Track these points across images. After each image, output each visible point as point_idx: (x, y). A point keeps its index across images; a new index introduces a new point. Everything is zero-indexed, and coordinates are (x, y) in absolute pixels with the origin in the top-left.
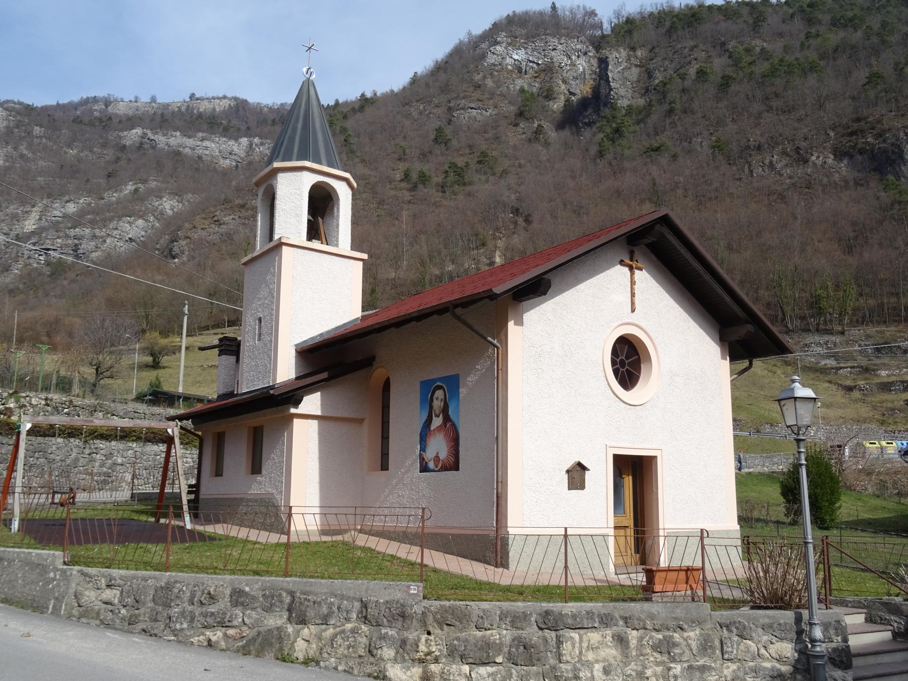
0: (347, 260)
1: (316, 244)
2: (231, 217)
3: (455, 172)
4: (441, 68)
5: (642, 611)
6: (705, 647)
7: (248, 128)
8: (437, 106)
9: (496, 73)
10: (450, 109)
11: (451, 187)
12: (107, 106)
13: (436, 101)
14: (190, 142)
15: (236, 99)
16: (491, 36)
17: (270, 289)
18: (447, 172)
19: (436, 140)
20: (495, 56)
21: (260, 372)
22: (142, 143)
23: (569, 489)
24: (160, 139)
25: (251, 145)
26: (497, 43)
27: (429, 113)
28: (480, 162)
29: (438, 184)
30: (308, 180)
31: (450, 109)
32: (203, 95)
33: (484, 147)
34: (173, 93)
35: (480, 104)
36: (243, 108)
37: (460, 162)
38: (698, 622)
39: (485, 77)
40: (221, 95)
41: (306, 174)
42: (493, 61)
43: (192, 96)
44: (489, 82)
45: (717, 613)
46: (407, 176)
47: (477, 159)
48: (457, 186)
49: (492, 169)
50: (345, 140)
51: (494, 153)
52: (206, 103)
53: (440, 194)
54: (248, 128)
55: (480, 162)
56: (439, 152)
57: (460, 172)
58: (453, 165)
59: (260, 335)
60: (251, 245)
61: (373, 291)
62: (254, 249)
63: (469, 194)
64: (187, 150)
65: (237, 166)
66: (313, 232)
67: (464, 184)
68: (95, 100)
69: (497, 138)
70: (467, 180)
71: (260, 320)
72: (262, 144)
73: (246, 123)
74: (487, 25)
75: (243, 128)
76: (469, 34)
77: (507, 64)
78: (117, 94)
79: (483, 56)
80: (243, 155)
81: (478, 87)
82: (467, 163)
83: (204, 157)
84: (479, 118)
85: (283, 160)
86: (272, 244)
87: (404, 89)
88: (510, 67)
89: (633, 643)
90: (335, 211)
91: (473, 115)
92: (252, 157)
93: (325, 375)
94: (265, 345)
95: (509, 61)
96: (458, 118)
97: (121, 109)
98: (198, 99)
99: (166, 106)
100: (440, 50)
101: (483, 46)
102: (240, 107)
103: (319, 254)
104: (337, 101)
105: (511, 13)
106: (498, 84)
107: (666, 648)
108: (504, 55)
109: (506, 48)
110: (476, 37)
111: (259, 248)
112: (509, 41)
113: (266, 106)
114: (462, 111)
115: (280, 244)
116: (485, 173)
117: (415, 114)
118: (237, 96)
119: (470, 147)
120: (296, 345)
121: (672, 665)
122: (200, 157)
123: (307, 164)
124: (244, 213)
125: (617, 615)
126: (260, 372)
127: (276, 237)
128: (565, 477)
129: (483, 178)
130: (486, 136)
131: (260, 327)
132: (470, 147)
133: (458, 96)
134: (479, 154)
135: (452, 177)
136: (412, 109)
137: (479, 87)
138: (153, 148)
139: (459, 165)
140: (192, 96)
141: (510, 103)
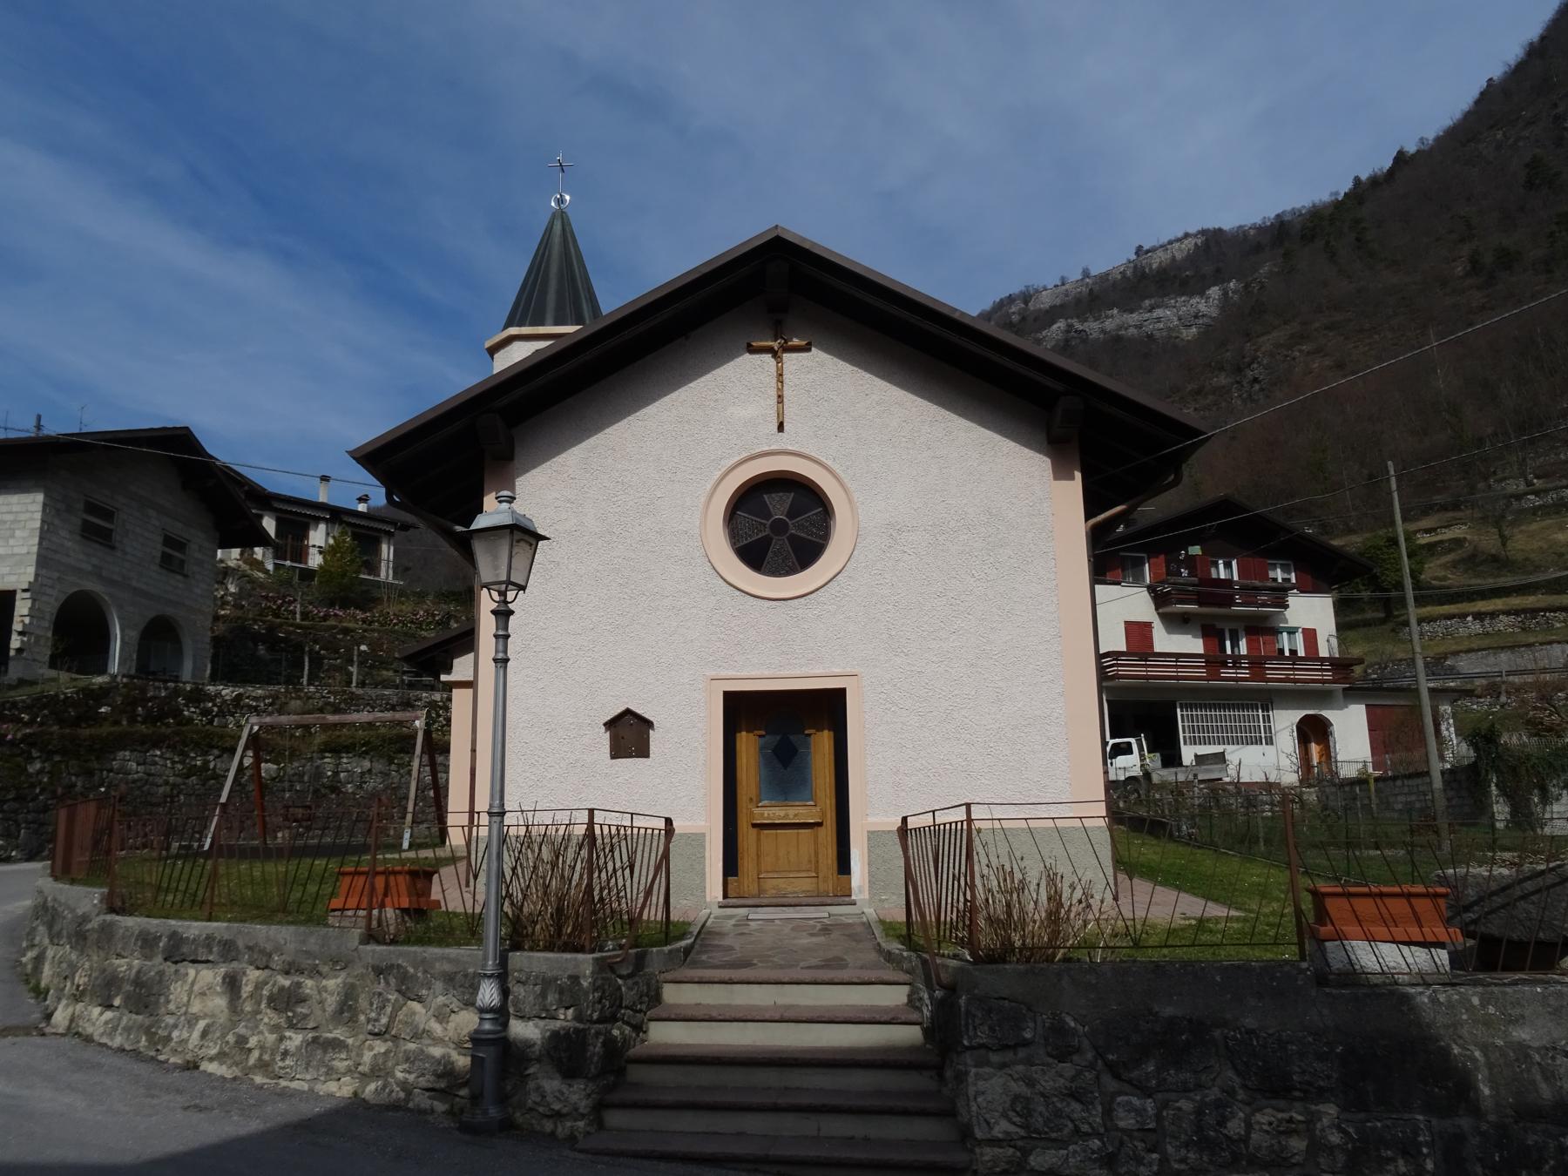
5: (268, 939)
6: (347, 1010)
12: (1026, 303)
14: (1134, 318)
15: (1203, 232)
22: (1067, 341)
23: (613, 757)
24: (1092, 327)
25: (1225, 294)
32: (1155, 243)
34: (1109, 256)
38: (340, 962)
40: (1180, 235)
41: (517, 345)
43: (1139, 250)
45: (369, 948)
46: (1475, 265)
50: (1358, 240)
52: (1160, 253)
64: (1132, 331)
68: (1011, 299)
78: (1038, 282)
83: (1157, 334)
89: (247, 990)
97: (1045, 301)
98: (1148, 251)
99: (1104, 277)
102: (1213, 241)
107: (286, 1001)
121: (287, 1034)
122: (1150, 337)
125: (240, 944)
128: (605, 738)
138: (1085, 341)
140: (1139, 250)
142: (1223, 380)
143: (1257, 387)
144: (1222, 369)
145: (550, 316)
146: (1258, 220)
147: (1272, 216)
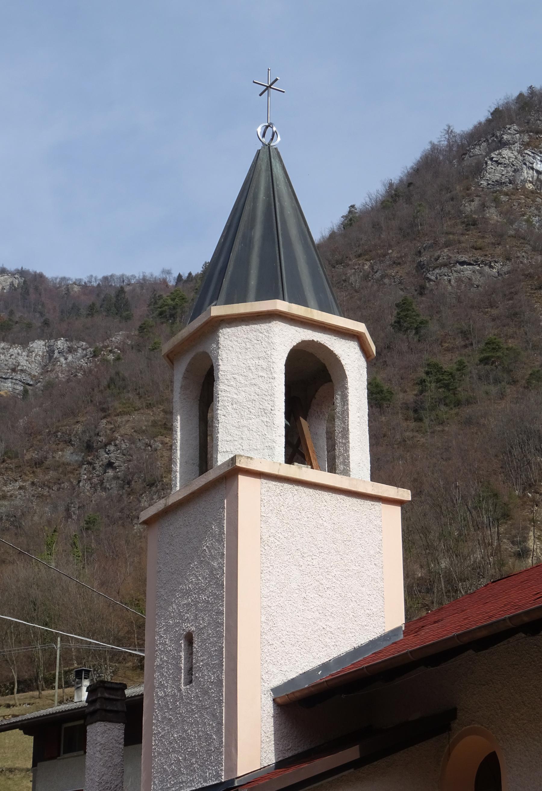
0: (369, 503)
1: (298, 471)
2: (17, 485)
3: (438, 381)
4: (397, 196)
7: (46, 323)
8: (396, 263)
9: (504, 198)
10: (420, 266)
11: (433, 408)
13: (393, 253)
15: (22, 273)
16: (491, 131)
17: (212, 569)
18: (423, 381)
19: (398, 325)
20: (500, 168)
21: (193, 754)
25: (51, 352)
26: (502, 144)
27: (383, 277)
28: (485, 361)
29: (406, 406)
30: (284, 338)
31: (420, 266)
33: (490, 333)
35: (478, 255)
36: (36, 289)
37: (447, 362)
39: (483, 206)
41: (278, 326)
42: (497, 176)
44: (493, 215)
47: (477, 357)
48: (443, 408)
49: (509, 371)
51: (511, 343)
53: (413, 424)
54: (46, 323)
55: (485, 361)
56: (404, 347)
57: (447, 382)
58: (434, 369)
59: (190, 671)
60: (158, 484)
61: (407, 574)
62: (168, 487)
63: (469, 422)
65: (26, 392)
66: (296, 452)
67: (458, 404)
69: (514, 315)
70: (462, 395)
71: (189, 639)
72: (70, 350)
73: (42, 314)
74: (482, 115)
75: (38, 323)
76: (449, 132)
77: (524, 181)
79: (479, 169)
80: (36, 370)
81: (471, 223)
82: (461, 363)
84: (477, 279)
85: (229, 301)
86: (211, 475)
87: (333, 235)
88: (530, 186)
90: (338, 398)
91: (466, 275)
92: (53, 375)
93: (352, 753)
94: (205, 692)
95: (527, 174)
96: (437, 282)
100: (394, 162)
101: (477, 151)
103: (311, 491)
104: (190, 274)
105: (525, 90)
106: (510, 216)
108: (518, 164)
109: (519, 152)
110: (462, 137)
111: (179, 488)
112: (526, 139)
113: (78, 283)
114: (445, 270)
115: (234, 471)
116: (497, 381)
117: (355, 280)
118: (26, 267)
119: (465, 334)
120: (275, 690)
123: (281, 305)
124: (41, 476)
126: (193, 754)
127: (222, 458)
129: (494, 390)
130: (495, 312)
131: (190, 653)
132: (465, 334)
133: (436, 243)
134: (482, 346)
135: (433, 391)
136: (350, 272)
137: (474, 223)
139: (446, 367)
141: (534, 249)
142: (69, 455)
143: (110, 473)
144: (69, 442)
145: (252, 292)
146: (84, 278)
147: (100, 277)
